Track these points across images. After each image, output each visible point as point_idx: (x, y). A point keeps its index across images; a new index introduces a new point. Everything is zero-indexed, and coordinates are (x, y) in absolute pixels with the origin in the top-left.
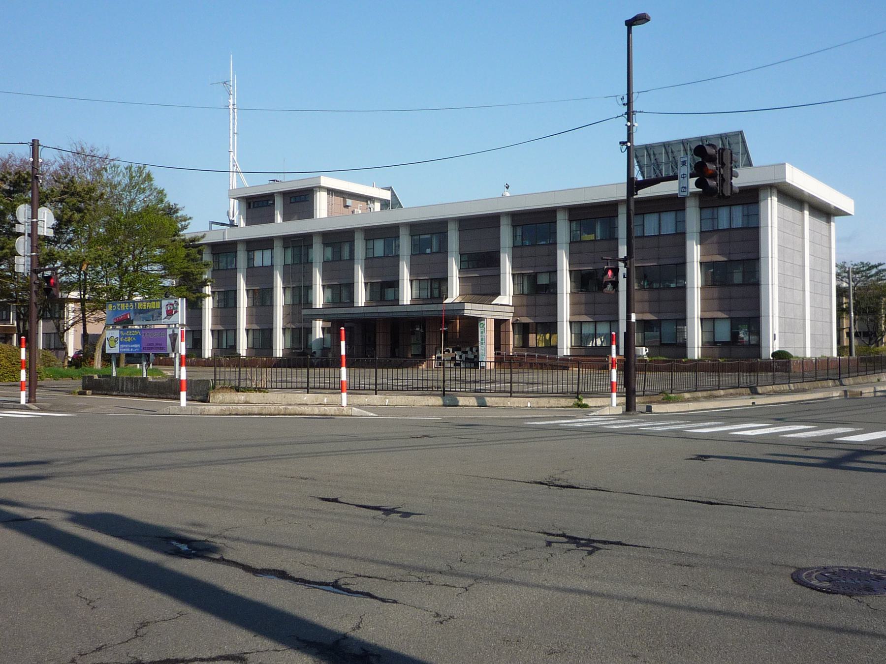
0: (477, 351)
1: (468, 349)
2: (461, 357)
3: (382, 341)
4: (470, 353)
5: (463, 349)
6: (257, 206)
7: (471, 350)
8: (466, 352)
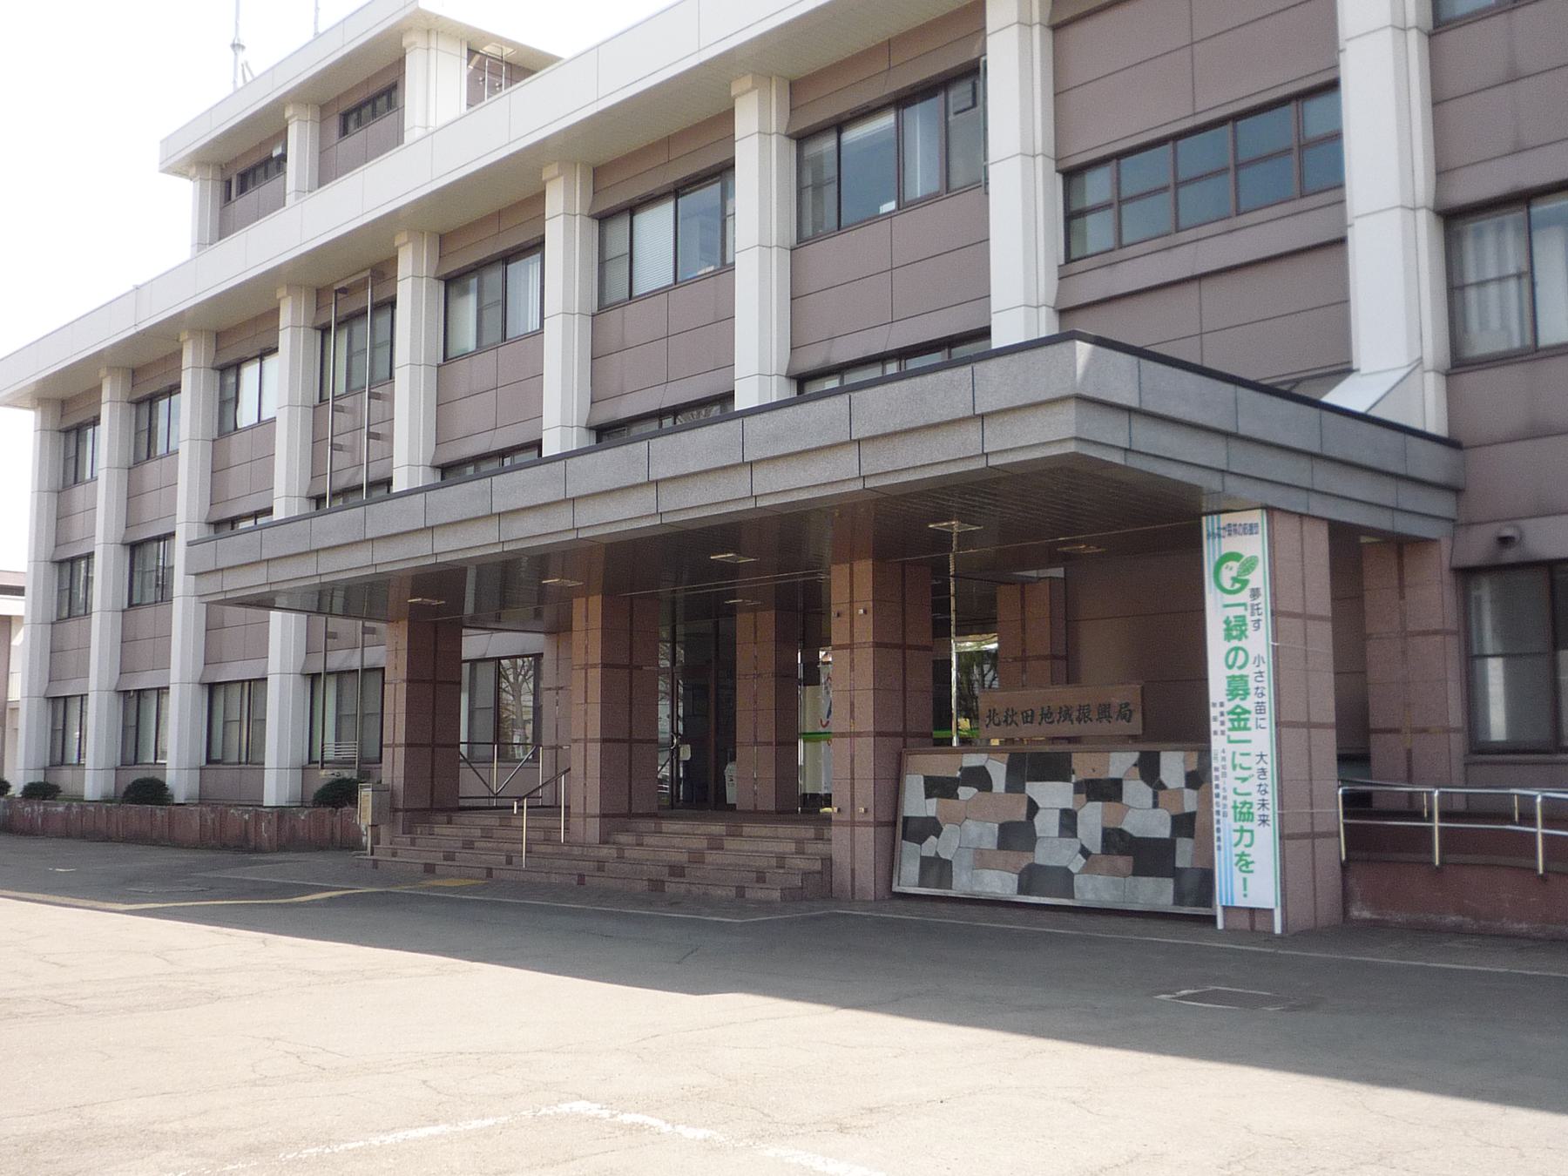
0: (1198, 779)
1: (1121, 763)
2: (1068, 821)
3: (550, 697)
4: (1136, 792)
5: (1085, 765)
6: (240, 170)
7: (1149, 769)
8: (1105, 790)
